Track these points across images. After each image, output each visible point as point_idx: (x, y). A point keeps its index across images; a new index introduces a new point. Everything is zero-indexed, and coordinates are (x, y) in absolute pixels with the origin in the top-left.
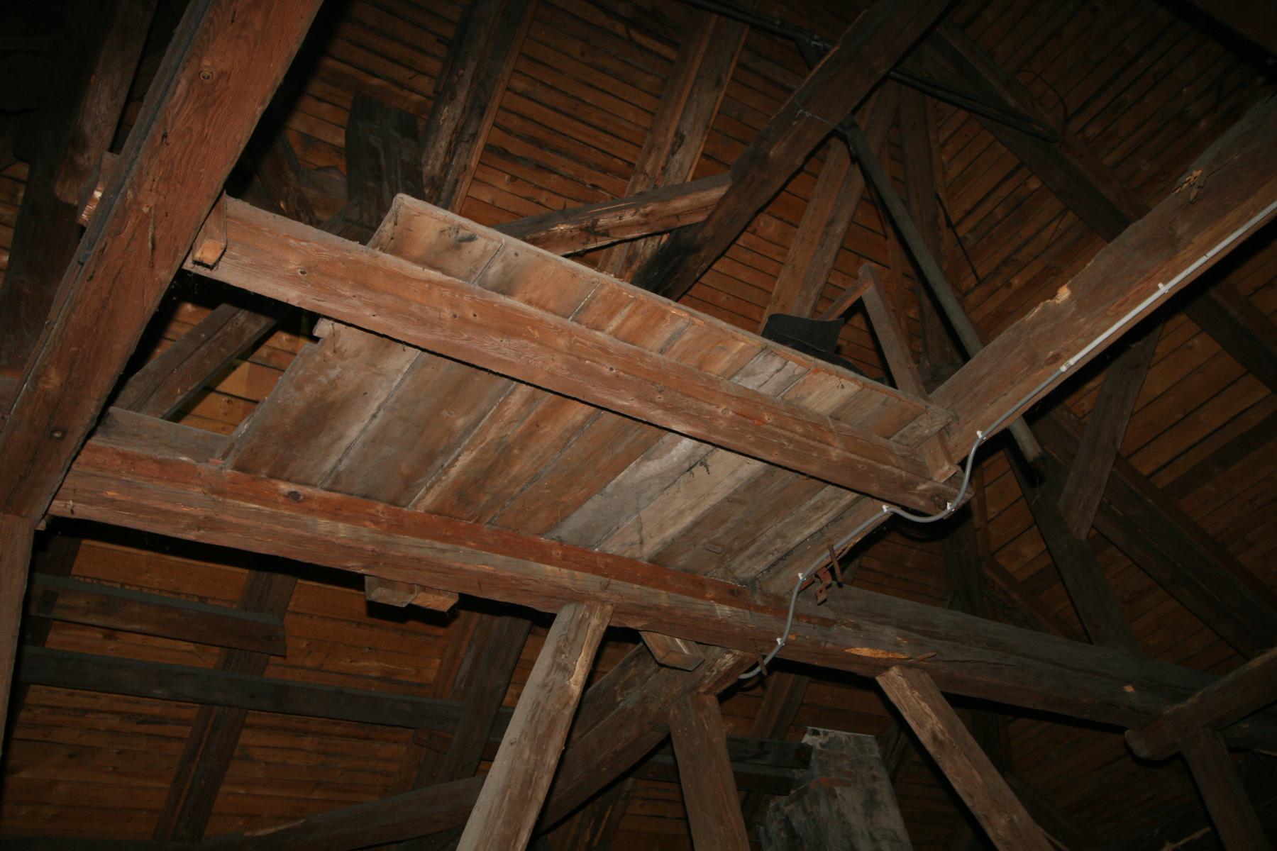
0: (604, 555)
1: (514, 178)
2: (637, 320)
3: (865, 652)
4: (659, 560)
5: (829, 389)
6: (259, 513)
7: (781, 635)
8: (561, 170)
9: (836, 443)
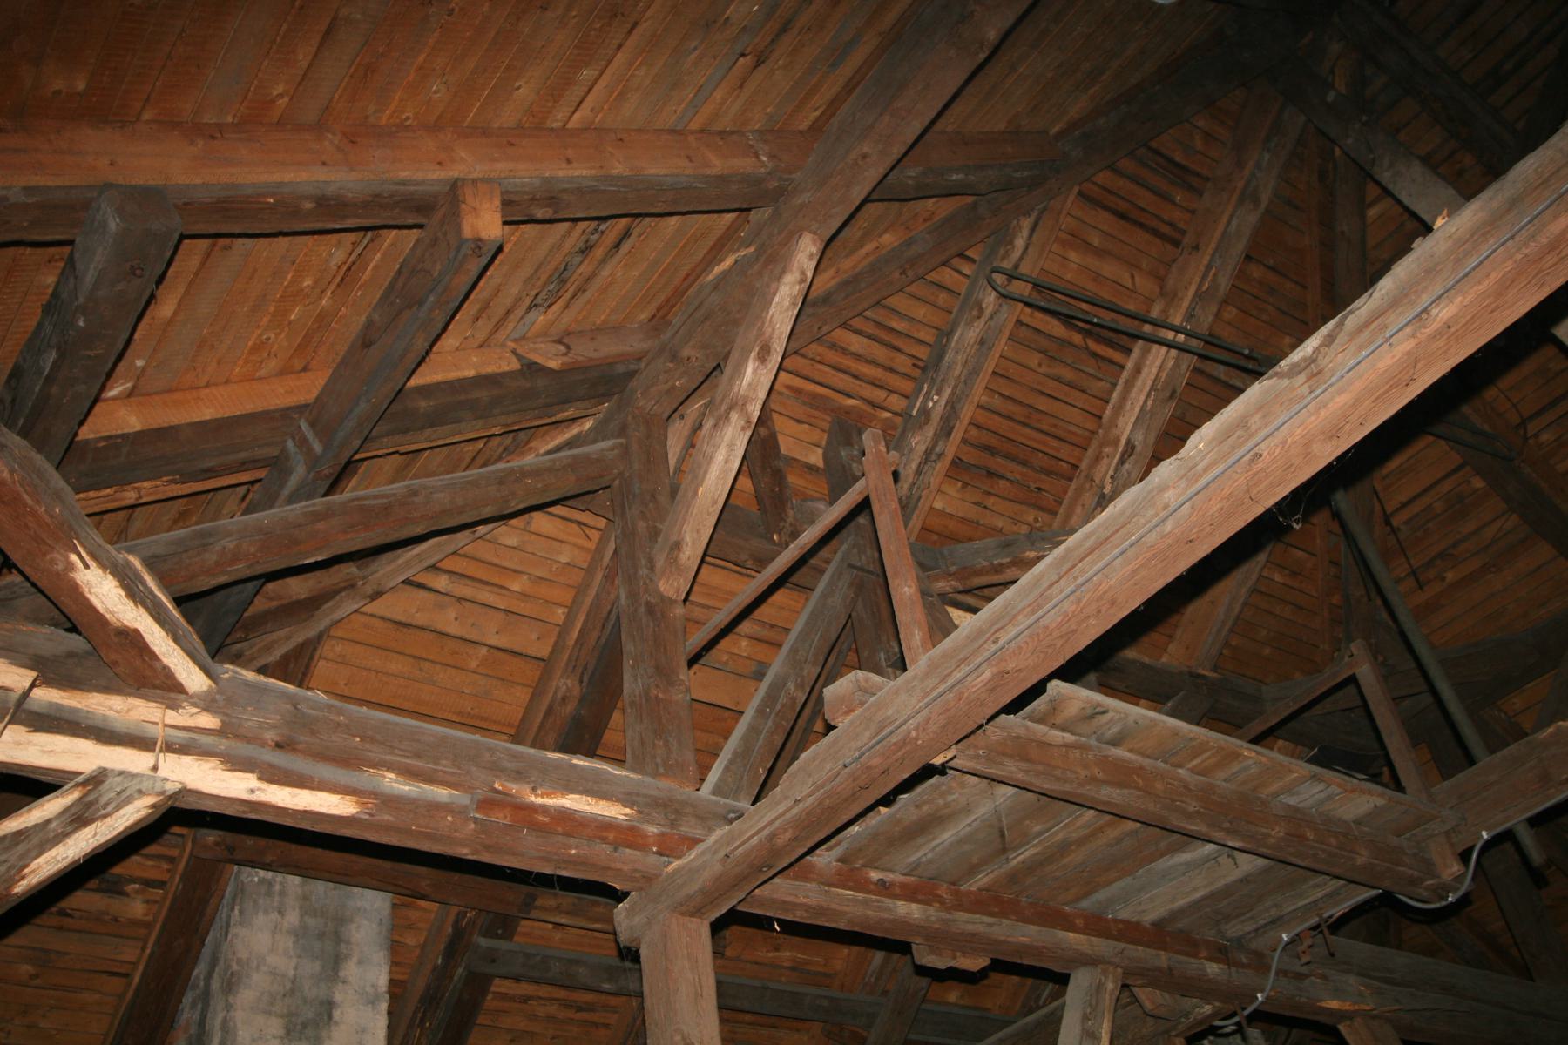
0: (1115, 921)
1: (965, 485)
2: (1214, 760)
3: (1334, 1004)
4: (1159, 925)
5: (1352, 801)
6: (855, 900)
7: (1262, 991)
8: (1009, 475)
9: (1364, 852)
